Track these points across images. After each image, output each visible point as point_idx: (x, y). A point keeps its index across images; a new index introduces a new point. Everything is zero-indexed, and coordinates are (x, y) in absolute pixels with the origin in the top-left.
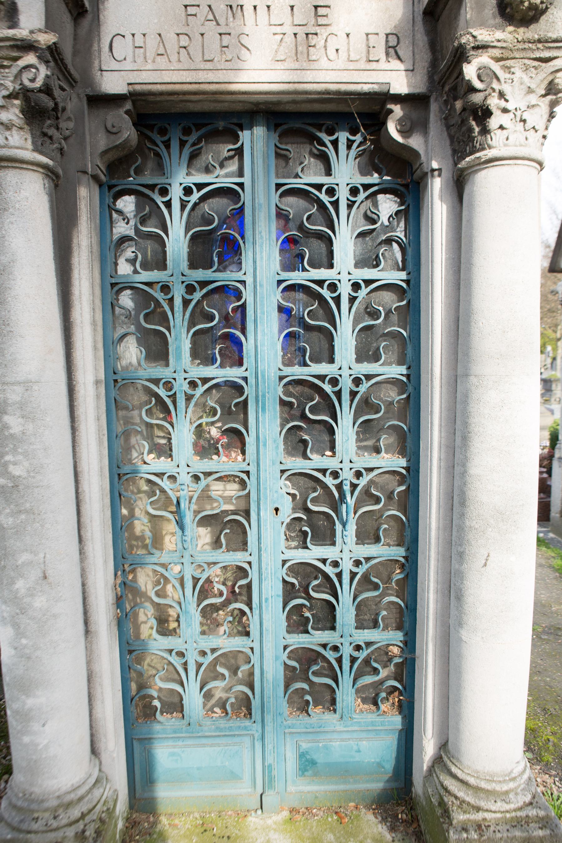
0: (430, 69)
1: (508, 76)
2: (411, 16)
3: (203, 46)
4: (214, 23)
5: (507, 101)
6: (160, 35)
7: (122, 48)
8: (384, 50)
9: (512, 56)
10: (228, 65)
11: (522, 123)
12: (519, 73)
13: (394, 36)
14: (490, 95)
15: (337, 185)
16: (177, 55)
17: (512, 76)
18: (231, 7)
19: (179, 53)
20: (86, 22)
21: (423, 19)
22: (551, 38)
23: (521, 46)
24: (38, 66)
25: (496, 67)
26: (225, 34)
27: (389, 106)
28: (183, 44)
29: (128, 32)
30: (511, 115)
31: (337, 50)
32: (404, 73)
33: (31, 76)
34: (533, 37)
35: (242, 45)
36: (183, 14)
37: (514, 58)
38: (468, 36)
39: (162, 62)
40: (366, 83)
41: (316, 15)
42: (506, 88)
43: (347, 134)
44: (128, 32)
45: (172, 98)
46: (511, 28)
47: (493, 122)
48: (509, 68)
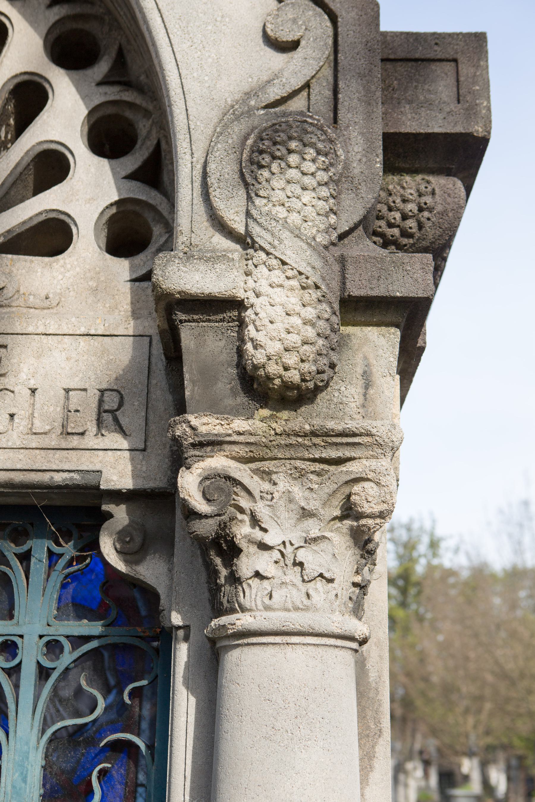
1: (266, 486)
2: (147, 362)
5: (265, 530)
8: (95, 417)
9: (270, 455)
11: (298, 569)
12: (283, 483)
13: (115, 394)
15: (21, 636)
21: (166, 369)
22: (333, 430)
25: (242, 472)
27: (104, 507)
31: (12, 416)
32: (127, 454)
37: (276, 459)
38: (184, 426)
40: (58, 471)
42: (262, 510)
43: (49, 543)
46: (265, 412)
47: (246, 565)
48: (269, 473)
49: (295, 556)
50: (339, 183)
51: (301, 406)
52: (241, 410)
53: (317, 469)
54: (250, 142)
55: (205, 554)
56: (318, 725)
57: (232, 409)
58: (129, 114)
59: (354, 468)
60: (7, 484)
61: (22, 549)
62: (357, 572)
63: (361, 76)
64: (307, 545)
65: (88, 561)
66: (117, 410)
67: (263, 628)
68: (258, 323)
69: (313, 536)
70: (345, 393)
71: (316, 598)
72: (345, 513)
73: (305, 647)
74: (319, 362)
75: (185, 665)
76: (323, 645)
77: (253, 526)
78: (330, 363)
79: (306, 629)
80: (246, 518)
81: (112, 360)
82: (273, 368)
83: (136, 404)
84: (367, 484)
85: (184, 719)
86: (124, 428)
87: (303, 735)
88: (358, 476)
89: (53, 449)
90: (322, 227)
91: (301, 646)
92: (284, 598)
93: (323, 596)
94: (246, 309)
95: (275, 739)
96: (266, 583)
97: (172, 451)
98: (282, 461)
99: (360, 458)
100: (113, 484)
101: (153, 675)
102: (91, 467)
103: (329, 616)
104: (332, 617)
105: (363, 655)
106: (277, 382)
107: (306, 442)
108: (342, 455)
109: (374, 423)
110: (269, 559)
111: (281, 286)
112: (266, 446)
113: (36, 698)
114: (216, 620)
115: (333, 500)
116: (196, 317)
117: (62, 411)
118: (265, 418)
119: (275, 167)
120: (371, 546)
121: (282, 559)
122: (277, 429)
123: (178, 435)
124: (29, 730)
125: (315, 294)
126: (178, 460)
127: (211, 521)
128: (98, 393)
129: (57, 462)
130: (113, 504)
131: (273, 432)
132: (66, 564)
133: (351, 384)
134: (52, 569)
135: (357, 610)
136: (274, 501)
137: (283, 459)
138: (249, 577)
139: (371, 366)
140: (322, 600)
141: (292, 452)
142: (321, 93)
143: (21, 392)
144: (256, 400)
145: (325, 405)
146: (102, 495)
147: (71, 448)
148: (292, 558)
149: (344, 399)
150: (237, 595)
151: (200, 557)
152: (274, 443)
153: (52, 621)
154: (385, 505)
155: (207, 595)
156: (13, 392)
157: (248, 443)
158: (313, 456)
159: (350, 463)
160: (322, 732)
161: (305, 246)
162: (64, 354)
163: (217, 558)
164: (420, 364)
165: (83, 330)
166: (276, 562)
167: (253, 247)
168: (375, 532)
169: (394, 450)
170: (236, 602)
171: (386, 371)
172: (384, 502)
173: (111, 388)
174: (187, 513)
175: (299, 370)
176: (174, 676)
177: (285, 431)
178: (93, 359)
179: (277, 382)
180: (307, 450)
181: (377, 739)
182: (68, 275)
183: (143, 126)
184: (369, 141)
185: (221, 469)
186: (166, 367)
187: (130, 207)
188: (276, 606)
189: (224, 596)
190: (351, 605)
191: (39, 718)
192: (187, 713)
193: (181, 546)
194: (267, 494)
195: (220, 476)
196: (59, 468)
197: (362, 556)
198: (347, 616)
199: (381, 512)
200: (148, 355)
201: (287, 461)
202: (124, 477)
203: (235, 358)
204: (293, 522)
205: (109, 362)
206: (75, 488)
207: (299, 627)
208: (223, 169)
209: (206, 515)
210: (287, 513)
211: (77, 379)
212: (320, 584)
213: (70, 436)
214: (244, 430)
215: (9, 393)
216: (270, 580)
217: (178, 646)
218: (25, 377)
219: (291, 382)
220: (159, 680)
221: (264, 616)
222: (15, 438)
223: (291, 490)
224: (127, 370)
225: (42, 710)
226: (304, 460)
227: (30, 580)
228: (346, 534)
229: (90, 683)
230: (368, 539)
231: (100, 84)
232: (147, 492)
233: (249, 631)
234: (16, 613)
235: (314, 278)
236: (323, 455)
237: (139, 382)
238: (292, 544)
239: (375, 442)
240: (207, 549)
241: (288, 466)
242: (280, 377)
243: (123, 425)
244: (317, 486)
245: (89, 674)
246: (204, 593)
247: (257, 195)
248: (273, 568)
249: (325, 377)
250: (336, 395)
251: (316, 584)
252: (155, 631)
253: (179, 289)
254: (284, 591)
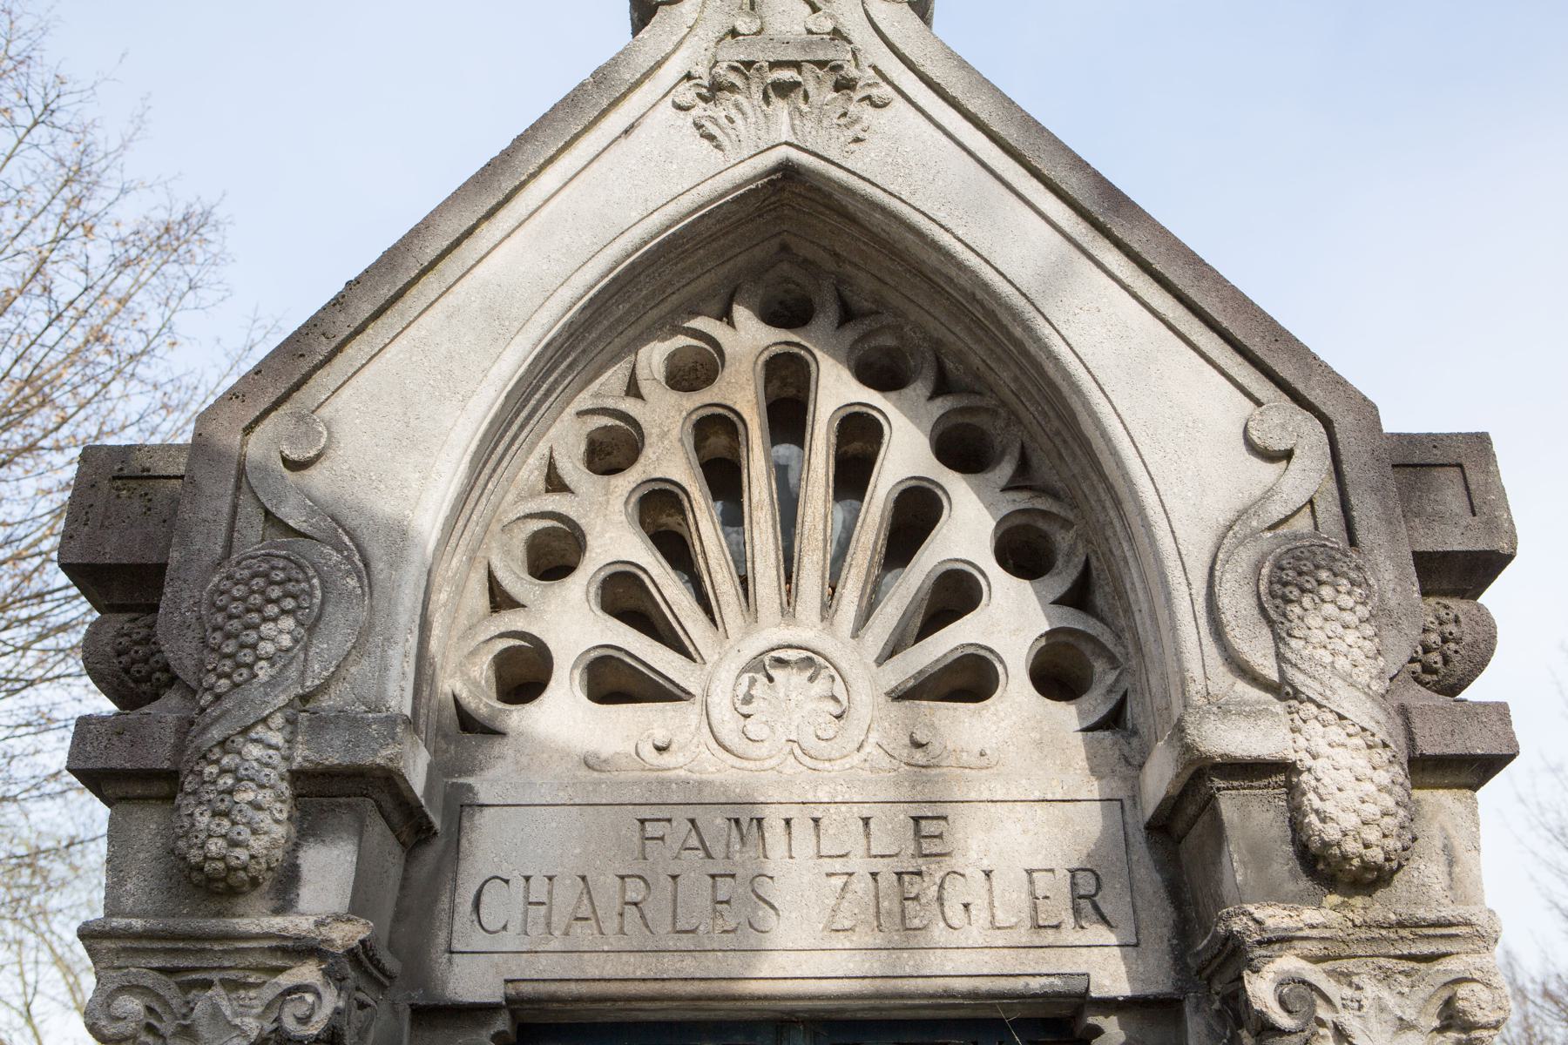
0: (1175, 942)
1: (1348, 992)
3: (675, 901)
4: (701, 854)
6: (583, 878)
7: (501, 907)
8: (1069, 905)
9: (1348, 952)
10: (729, 941)
16: (617, 919)
17: (1357, 994)
18: (737, 821)
19: (621, 915)
20: (430, 854)
23: (1363, 934)
24: (321, 989)
25: (1315, 974)
26: (721, 876)
27: (1091, 1020)
28: (632, 895)
29: (516, 873)
31: (966, 906)
32: (1117, 951)
33: (302, 1010)
35: (759, 897)
36: (636, 838)
39: (584, 935)
40: (1033, 975)
41: (917, 831)
44: (516, 873)
45: (601, 1006)
46: (1334, 899)
48: (1348, 975)
50: (1381, 617)
54: (1265, 571)
58: (1041, 524)
59: (1455, 966)
63: (1374, 490)
68: (1322, 790)
90: (1375, 672)
94: (1300, 773)
102: (1075, 970)
106: (1356, 862)
111: (1343, 745)
116: (1236, 784)
119: (1306, 601)
125: (1387, 754)
142: (1329, 510)
159: (1448, 959)
161: (1363, 697)
165: (1037, 795)
167: (1295, 698)
179: (1356, 862)
182: (1002, 724)
183: (1063, 540)
184: (1398, 566)
187: (1062, 638)
204: (1388, 1036)
208: (1237, 603)
211: (1040, 857)
224: (1100, 843)
231: (1004, 490)
235: (1381, 735)
242: (1361, 856)
247: (1290, 635)
253: (1220, 751)
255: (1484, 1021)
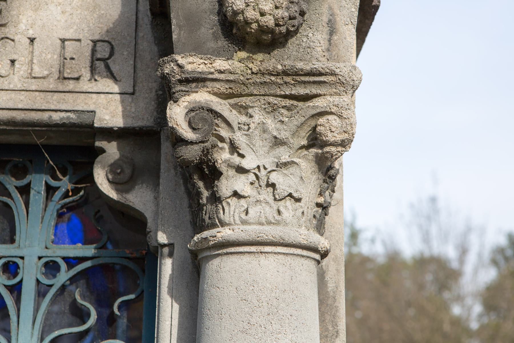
1: (244, 119)
5: (242, 156)
8: (88, 64)
9: (247, 91)
11: (270, 190)
12: (258, 116)
13: (106, 44)
14: (214, 146)
15: (22, 258)
21: (152, 24)
22: (302, 70)
23: (258, 79)
27: (98, 144)
30: (252, 177)
31: (13, 62)
32: (118, 97)
34: (274, 67)
37: (252, 95)
38: (172, 64)
42: (240, 138)
46: (243, 54)
47: (226, 186)
48: (246, 108)
49: (268, 178)
51: (274, 50)
52: (222, 52)
53: (287, 105)
55: (187, 180)
56: (287, 321)
57: (214, 51)
59: (320, 103)
60: (9, 122)
61: (22, 182)
62: (320, 194)
64: (279, 169)
65: (82, 193)
66: (108, 59)
67: (241, 239)
69: (284, 161)
70: (313, 39)
71: (287, 215)
72: (311, 143)
73: (276, 256)
74: (291, 9)
75: (170, 277)
76: (292, 254)
77: (232, 153)
78: (300, 11)
79: (277, 239)
80: (226, 146)
81: (103, 14)
82: (251, 14)
83: (125, 53)
84: (331, 117)
85: (168, 323)
86: (115, 75)
87: (275, 329)
88: (323, 110)
89: (52, 92)
91: (272, 254)
92: (258, 214)
93: (292, 213)
95: (250, 332)
96: (243, 201)
97: (157, 95)
98: (257, 97)
99: (324, 95)
100: (105, 122)
101: (139, 291)
102: (86, 108)
103: (297, 229)
104: (299, 230)
105: (322, 269)
106: (254, 26)
107: (278, 80)
108: (309, 92)
109: (338, 65)
110: (246, 181)
112: (243, 84)
113: (36, 310)
114: (198, 235)
115: (301, 132)
117: (59, 59)
118: (243, 59)
120: (332, 172)
121: (257, 181)
122: (253, 69)
123: (167, 73)
124: (29, 338)
126: (165, 93)
127: (196, 147)
128: (91, 43)
129: (55, 103)
130: (105, 140)
131: (249, 71)
132: (62, 195)
133: (318, 31)
134: (49, 201)
135: (320, 227)
136: (251, 130)
137: (258, 95)
138: (228, 196)
139: (335, 15)
140: (291, 216)
141: (266, 89)
143: (21, 40)
144: (235, 43)
145: (295, 49)
146: (95, 134)
147: (68, 90)
148: (266, 180)
149: (312, 44)
150: (217, 212)
151: (182, 186)
152: (250, 81)
153: (50, 245)
154: (346, 135)
155: (188, 218)
156: (13, 40)
157: (228, 81)
158: (284, 93)
159: (316, 99)
160: (290, 327)
162: (59, 8)
163: (200, 182)
164: (373, 23)
166: (252, 184)
168: (336, 159)
169: (354, 88)
170: (216, 218)
171: (348, 20)
172: (345, 132)
173: (102, 39)
174: (175, 141)
175: (274, 16)
176: (159, 287)
177: (260, 71)
178: (86, 13)
179: (254, 26)
180: (279, 87)
181: (334, 339)
185: (205, 103)
186: (152, 21)
188: (251, 221)
189: (206, 214)
190: (315, 222)
191: (38, 327)
192: (171, 318)
193: (167, 175)
194: (244, 125)
195: (203, 109)
196: (57, 108)
197: (325, 181)
198: (311, 231)
199: (343, 141)
200: (135, 11)
201: (262, 97)
202: (116, 116)
203: (217, 6)
204: (266, 149)
205: (100, 16)
206: (71, 127)
207: (271, 238)
209: (191, 142)
210: (261, 142)
211: (72, 31)
212: (289, 202)
213: (67, 81)
214: (224, 68)
215: (10, 41)
216: (247, 199)
217: (163, 262)
218: (24, 28)
219: (267, 26)
220: (145, 295)
221: (241, 229)
222: (16, 80)
223: (265, 122)
224: (118, 23)
225: (41, 321)
226: (277, 96)
227: (30, 209)
228: (312, 160)
229: (83, 297)
230: (330, 166)
232: (136, 130)
233: (229, 242)
234: (17, 238)
236: (293, 92)
237: (128, 35)
238: (265, 168)
239: (338, 81)
240: (190, 176)
241: (263, 102)
242: (257, 21)
243: (114, 72)
244: (287, 119)
245: (83, 291)
246: (186, 216)
248: (249, 188)
249: (296, 22)
250: (304, 40)
251: (285, 203)
252: (141, 253)
254: (258, 208)
255: (332, 140)
